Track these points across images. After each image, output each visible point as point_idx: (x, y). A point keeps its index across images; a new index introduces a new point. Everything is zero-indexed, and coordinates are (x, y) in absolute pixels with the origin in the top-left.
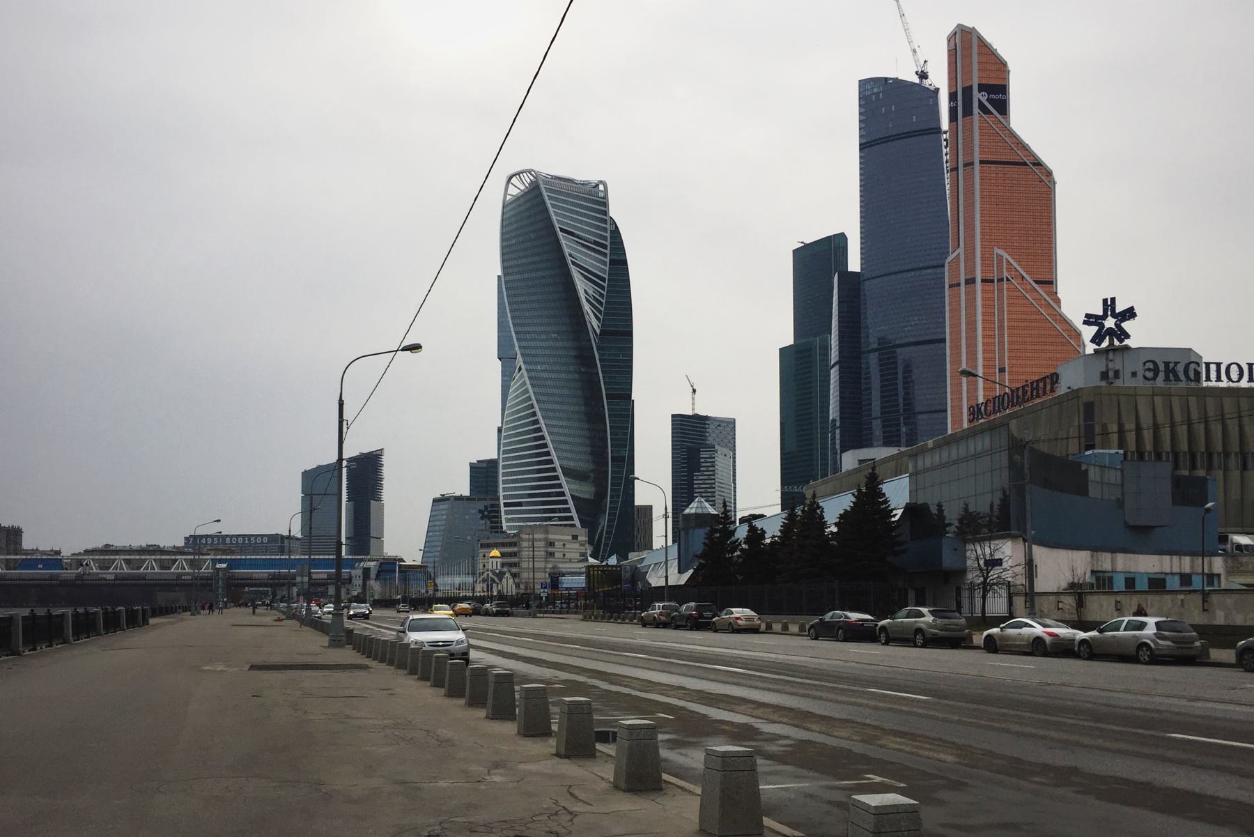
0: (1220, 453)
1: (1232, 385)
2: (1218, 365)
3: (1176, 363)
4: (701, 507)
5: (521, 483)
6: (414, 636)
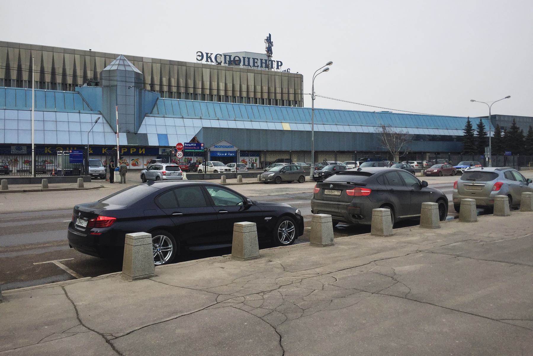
0: (231, 96)
3: (211, 54)
6: (167, 260)
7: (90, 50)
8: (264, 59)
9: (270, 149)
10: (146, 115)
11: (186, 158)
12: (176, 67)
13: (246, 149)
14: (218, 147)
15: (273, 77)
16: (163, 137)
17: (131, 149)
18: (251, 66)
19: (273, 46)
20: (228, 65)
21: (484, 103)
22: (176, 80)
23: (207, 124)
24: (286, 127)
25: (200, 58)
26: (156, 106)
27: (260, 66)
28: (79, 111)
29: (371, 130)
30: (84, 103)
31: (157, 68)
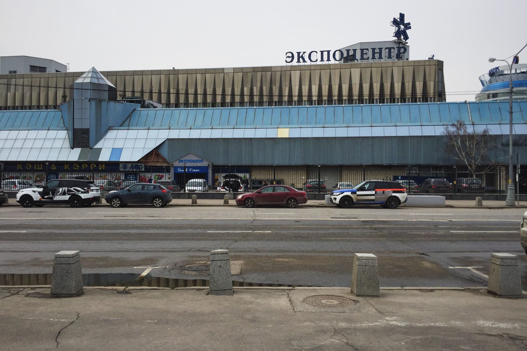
1: (312, 63)
2: (329, 52)
3: (304, 53)
4: (97, 78)
5: (410, 286)
7: (173, 68)
8: (351, 49)
9: (256, 163)
10: (109, 128)
11: (156, 175)
12: (259, 75)
13: (396, 163)
14: (183, 161)
15: (389, 70)
16: (117, 151)
17: (83, 165)
18: (357, 60)
19: (410, 28)
20: (344, 62)
21: (503, 60)
22: (268, 88)
23: (175, 134)
24: (284, 133)
25: (289, 60)
26: (128, 120)
27: (371, 57)
28: (149, 127)
29: (439, 131)
30: (62, 120)
31: (239, 76)
